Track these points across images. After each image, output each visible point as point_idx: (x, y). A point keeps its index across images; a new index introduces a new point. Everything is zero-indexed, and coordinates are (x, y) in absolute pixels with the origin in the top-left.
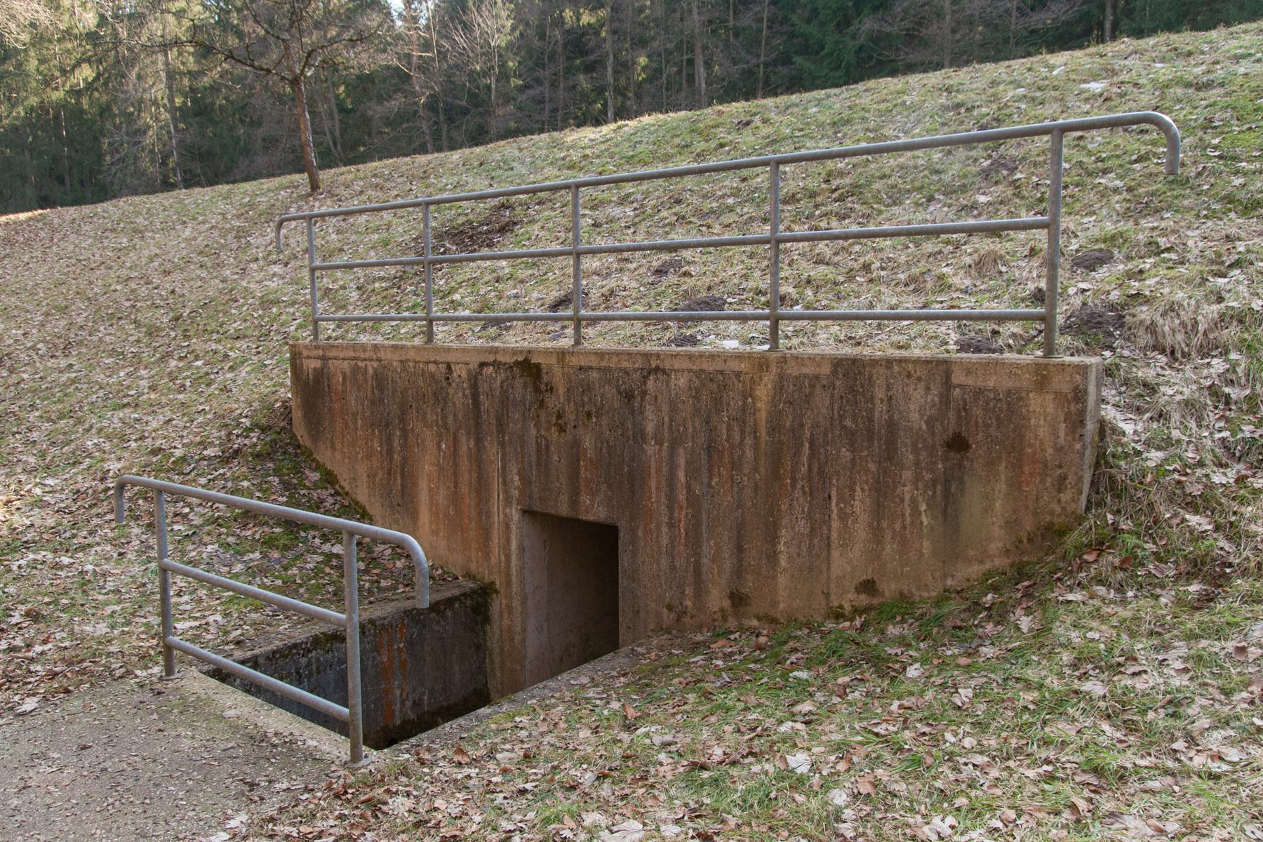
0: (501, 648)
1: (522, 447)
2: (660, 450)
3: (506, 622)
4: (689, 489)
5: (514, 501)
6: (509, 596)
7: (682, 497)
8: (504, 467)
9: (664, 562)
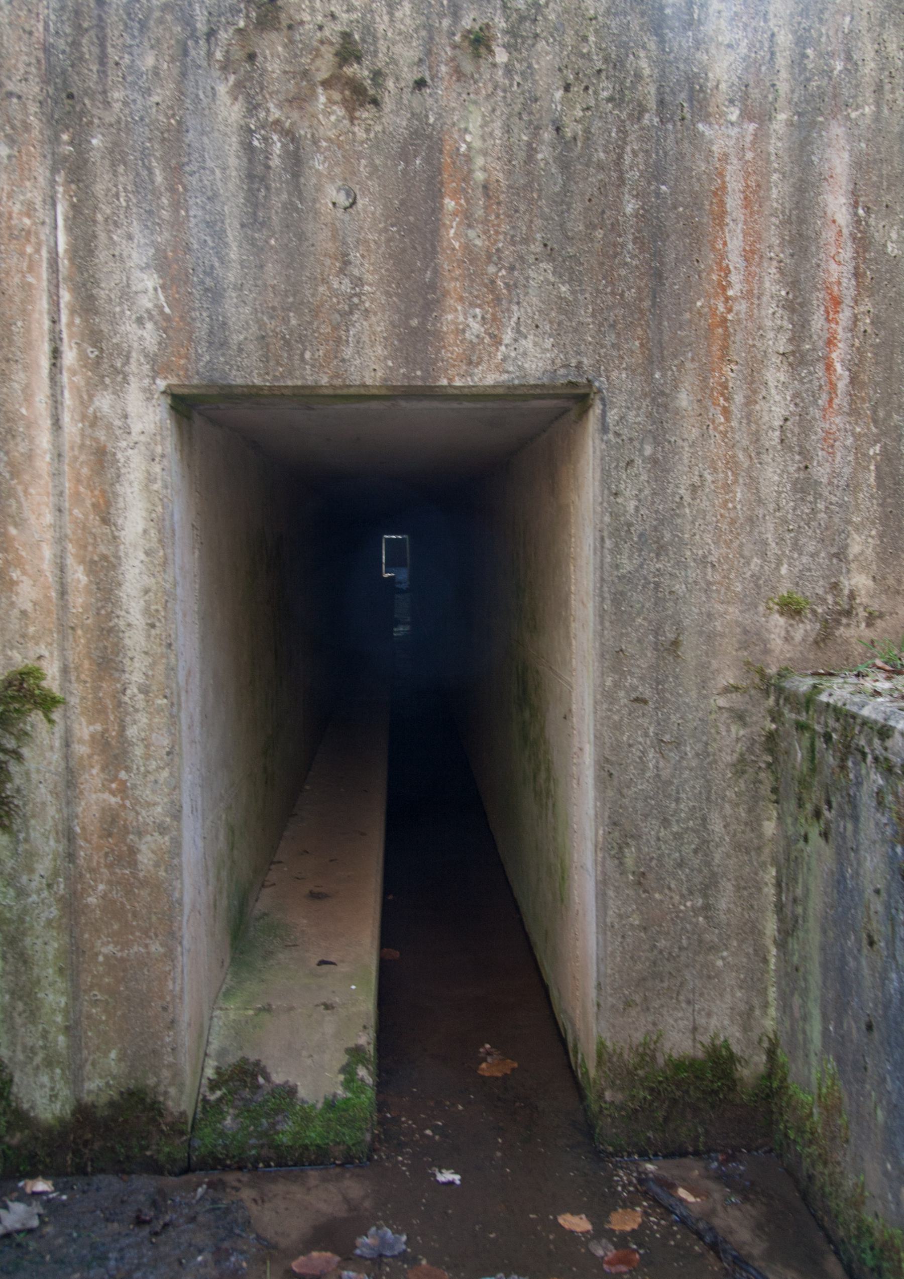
0: (72, 906)
1: (176, 171)
2: (760, 137)
3: (96, 796)
4: (862, 241)
5: (137, 367)
6: (111, 707)
7: (837, 267)
8: (84, 248)
9: (773, 474)
